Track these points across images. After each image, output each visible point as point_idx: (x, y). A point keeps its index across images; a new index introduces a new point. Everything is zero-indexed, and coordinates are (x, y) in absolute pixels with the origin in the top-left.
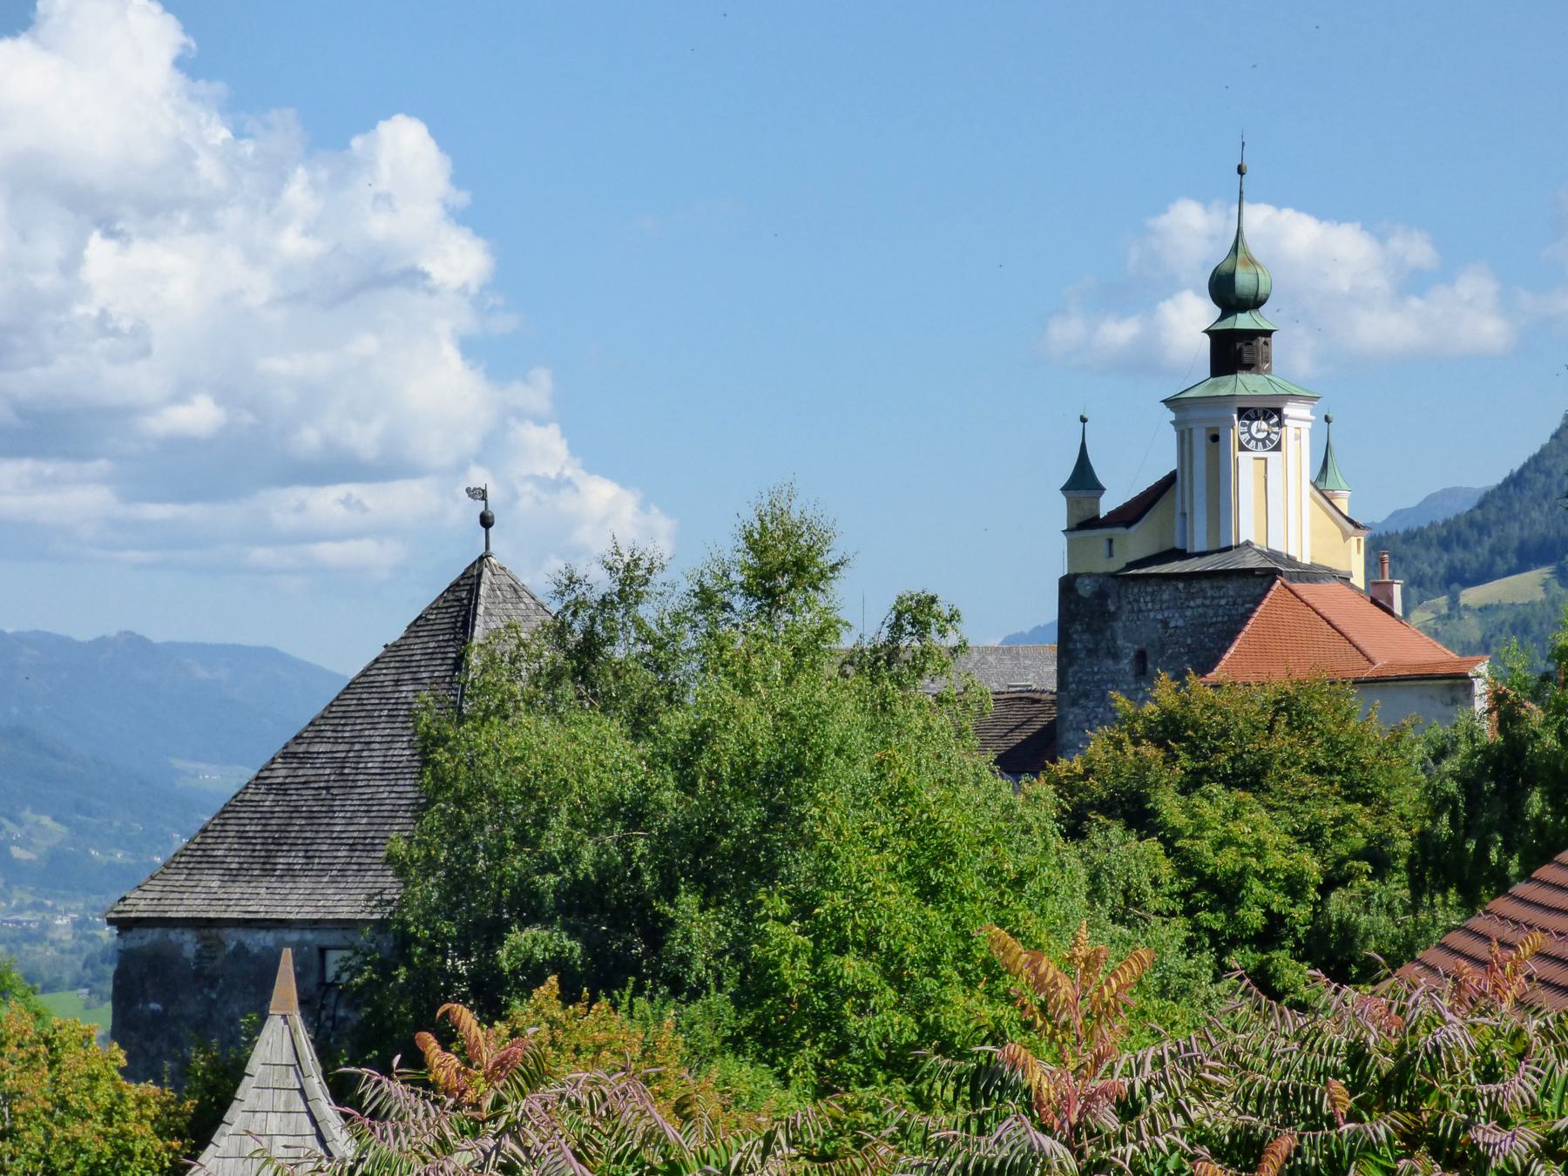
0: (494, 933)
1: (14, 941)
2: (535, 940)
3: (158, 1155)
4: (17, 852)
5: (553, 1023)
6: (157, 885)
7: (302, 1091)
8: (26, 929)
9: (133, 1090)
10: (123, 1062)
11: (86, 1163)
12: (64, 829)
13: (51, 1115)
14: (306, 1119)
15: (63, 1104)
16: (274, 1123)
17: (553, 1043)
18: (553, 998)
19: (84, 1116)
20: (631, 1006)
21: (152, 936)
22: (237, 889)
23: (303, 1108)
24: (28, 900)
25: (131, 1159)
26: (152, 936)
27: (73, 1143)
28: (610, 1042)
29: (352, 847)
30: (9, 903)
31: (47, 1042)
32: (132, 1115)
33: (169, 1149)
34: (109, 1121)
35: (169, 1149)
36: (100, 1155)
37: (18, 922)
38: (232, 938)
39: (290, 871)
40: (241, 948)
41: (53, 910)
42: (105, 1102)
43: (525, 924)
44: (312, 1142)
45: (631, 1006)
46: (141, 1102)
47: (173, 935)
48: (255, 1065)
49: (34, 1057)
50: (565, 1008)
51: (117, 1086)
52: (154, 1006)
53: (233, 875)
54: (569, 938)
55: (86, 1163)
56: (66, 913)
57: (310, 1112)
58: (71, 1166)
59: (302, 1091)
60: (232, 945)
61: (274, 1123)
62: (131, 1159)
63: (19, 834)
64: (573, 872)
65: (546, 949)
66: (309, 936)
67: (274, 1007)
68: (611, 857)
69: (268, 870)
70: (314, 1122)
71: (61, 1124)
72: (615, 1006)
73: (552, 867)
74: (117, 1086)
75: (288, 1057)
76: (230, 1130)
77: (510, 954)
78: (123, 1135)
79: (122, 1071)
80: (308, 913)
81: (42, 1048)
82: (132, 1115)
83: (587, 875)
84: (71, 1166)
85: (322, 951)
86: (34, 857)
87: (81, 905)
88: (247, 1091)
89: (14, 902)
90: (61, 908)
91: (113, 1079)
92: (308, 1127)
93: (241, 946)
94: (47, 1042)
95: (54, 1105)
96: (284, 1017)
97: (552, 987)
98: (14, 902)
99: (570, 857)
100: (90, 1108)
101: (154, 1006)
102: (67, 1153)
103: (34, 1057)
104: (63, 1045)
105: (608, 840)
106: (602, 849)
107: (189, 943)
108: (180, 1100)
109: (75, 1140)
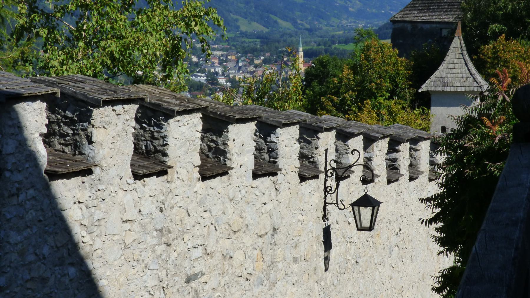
0: (486, 26)
1: (349, 30)
2: (496, 27)
3: (405, 74)
4: (351, 9)
5: (504, 45)
6: (402, 13)
7: (462, 54)
8: (352, 27)
9: (400, 59)
10: (398, 53)
11: (389, 75)
12: (361, 4)
13: (381, 64)
14: (463, 60)
15: (384, 62)
16: (455, 61)
17: (503, 50)
18: (503, 39)
19: (388, 64)
20: (520, 42)
21: (400, 25)
22: (421, 15)
23: (462, 58)
24: (353, 20)
25: (399, 75)
26: (400, 25)
27: (386, 71)
28: (517, 50)
29: (449, 5)
30: (348, 21)
31: (381, 47)
32: (400, 65)
33: (408, 73)
34: (394, 66)
35: (408, 73)
36: (392, 74)
37: (350, 26)
38: (419, 26)
39: (434, 11)
40: (422, 28)
41: (358, 23)
42: (393, 62)
43: (494, 23)
44: (464, 65)
45: (520, 42)
46: (402, 62)
47: (406, 25)
48: (452, 47)
49: (378, 51)
50: (506, 41)
51: (396, 58)
52: (401, 41)
53: (420, 11)
54: (504, 27)
55: (389, 75)
56: (361, 24)
57: (464, 59)
58: (386, 76)
59: (462, 54)
60: (419, 27)
61: (455, 61)
62: (399, 75)
63: (351, 5)
64: (506, 11)
65: (499, 29)
66: (438, 25)
67: (456, 35)
68: (516, 7)
69: (429, 10)
70: (465, 61)
71: (384, 66)
72: (517, 41)
73: (501, 9)
74: (396, 58)
75: (459, 46)
76: (445, 62)
77: (490, 30)
78: (397, 69)
79: (397, 55)
80: (437, 20)
81: (380, 49)
82: (400, 65)
83: (509, 12)
84: (386, 76)
85: (441, 29)
86: (354, 10)
87: (365, 22)
88: (449, 53)
89: (349, 21)
90: (360, 22)
91: (395, 56)
92: (463, 62)
93: (422, 28)
94: (381, 47)
95: (382, 62)
96: (458, 37)
97: (503, 37)
98: (349, 21)
99: (506, 7)
100: (390, 63)
101: (401, 41)
102: (385, 73)
103: (378, 51)
104: (384, 48)
105: (515, 3)
106: (513, 6)
107: (409, 27)
108: (410, 62)
109: (387, 70)
